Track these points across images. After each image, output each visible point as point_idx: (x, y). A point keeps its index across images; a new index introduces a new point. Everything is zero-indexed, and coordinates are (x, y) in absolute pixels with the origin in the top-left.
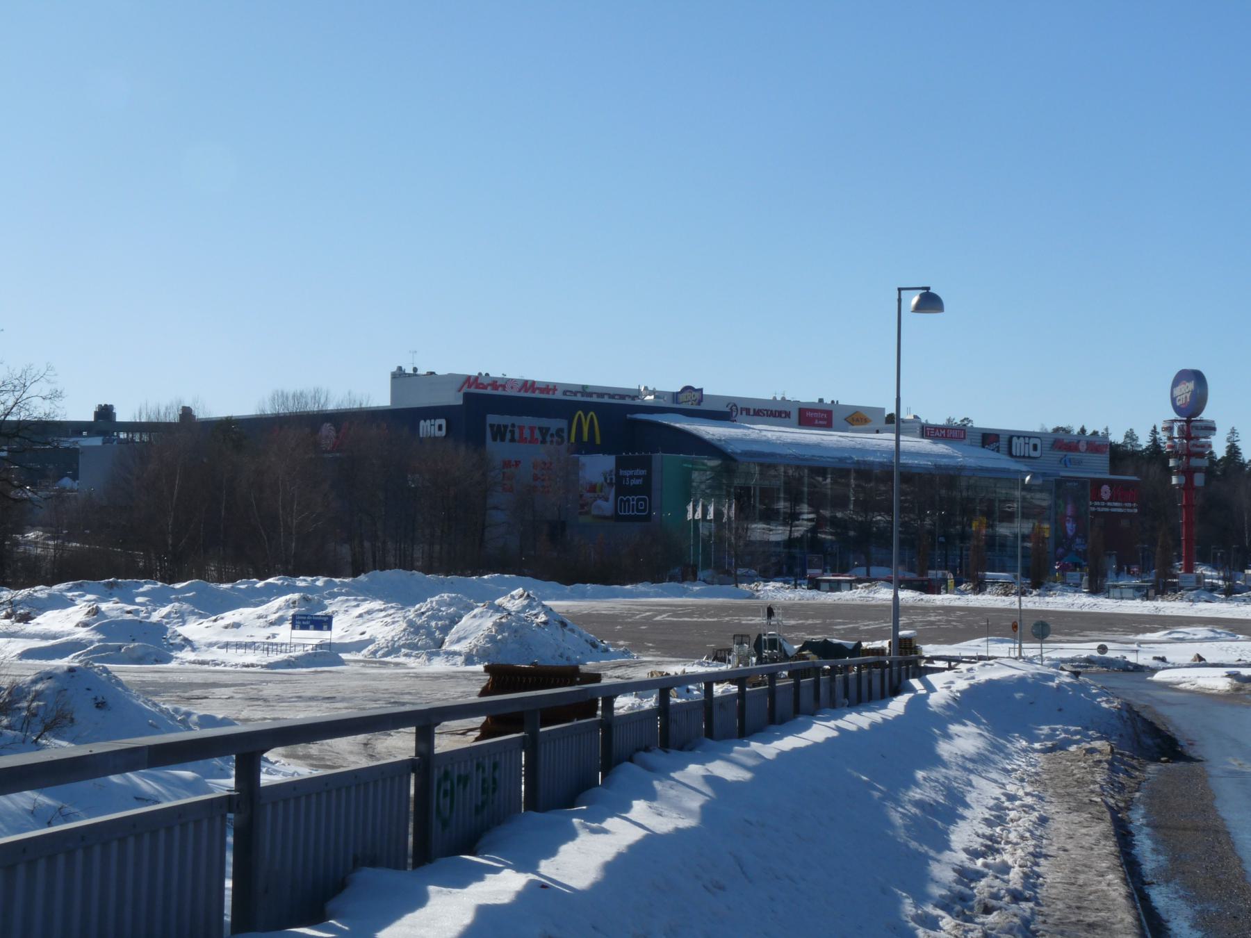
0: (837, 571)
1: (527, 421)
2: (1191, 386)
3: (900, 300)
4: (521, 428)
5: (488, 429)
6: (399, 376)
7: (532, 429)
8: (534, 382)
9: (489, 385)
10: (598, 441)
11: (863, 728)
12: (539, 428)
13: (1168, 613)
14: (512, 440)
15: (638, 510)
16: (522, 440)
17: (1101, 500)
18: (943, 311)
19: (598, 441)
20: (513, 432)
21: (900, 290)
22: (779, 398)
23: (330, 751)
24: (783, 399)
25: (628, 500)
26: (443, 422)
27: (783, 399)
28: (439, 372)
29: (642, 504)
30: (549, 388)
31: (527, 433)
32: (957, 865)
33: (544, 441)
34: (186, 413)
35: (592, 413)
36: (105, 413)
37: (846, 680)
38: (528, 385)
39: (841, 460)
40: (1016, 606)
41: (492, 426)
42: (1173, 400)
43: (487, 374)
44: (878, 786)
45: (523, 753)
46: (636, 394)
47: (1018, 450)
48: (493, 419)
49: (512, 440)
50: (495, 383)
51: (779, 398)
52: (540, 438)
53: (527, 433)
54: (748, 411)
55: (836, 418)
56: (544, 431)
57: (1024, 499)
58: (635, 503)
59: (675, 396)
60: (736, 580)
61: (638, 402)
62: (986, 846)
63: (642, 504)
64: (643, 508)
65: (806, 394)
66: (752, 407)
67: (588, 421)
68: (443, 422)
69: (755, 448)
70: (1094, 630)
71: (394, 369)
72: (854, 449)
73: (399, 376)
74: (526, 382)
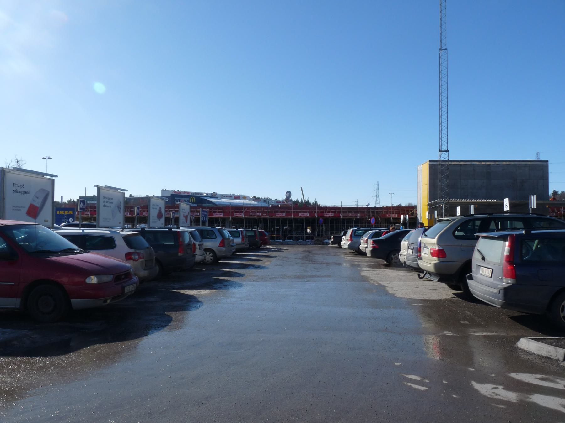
0: (408, 228)
1: (182, 199)
2: (289, 194)
5: (175, 201)
6: (163, 190)
10: (195, 202)
18: (80, 197)
19: (195, 202)
20: (179, 201)
30: (189, 193)
32: (317, 254)
34: (154, 195)
35: (194, 197)
36: (154, 195)
37: (271, 232)
38: (185, 192)
39: (237, 205)
40: (61, 211)
42: (286, 196)
46: (202, 194)
47: (532, 198)
48: (176, 198)
54: (225, 196)
61: (203, 195)
62: (305, 251)
65: (236, 193)
67: (193, 199)
69: (221, 203)
71: (162, 189)
72: (239, 203)
73: (163, 190)
74: (185, 192)
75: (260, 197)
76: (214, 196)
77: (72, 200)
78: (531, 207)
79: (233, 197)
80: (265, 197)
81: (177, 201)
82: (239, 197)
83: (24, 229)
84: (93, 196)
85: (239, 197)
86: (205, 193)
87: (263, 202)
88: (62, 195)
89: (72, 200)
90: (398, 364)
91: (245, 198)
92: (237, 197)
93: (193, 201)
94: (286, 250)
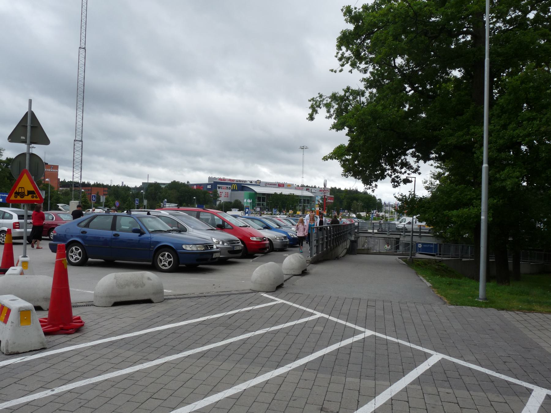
1: (224, 186)
5: (217, 187)
7: (225, 187)
10: (237, 189)
13: (394, 339)
14: (222, 189)
16: (223, 189)
19: (237, 189)
23: (340, 242)
26: (210, 186)
31: (224, 188)
33: (227, 189)
41: (218, 187)
44: (55, 328)
45: (473, 259)
46: (245, 181)
48: (218, 185)
49: (222, 189)
53: (224, 188)
56: (227, 187)
57: (304, 205)
60: (373, 228)
66: (270, 183)
68: (210, 186)
70: (468, 306)
75: (396, 188)
76: (258, 183)
77: (126, 186)
78: (204, 250)
79: (277, 185)
80: (312, 186)
81: (219, 188)
82: (284, 185)
83: (466, 210)
84: (154, 182)
85: (284, 185)
86: (248, 181)
87: (306, 190)
88: (123, 181)
89: (126, 186)
90: (472, 140)
91: (289, 186)
92: (281, 185)
93: (234, 189)
94: (464, 409)
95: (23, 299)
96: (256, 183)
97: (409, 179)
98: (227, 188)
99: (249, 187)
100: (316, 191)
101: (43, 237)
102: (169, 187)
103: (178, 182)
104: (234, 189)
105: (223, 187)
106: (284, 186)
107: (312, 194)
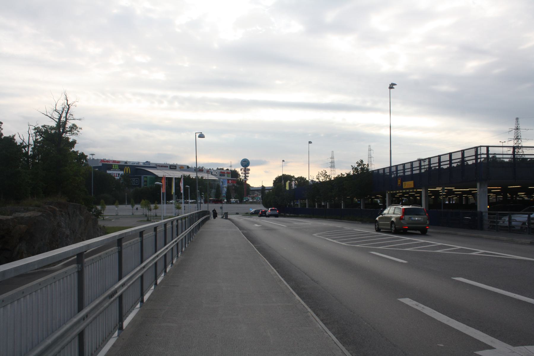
3: (196, 135)
4: (114, 174)
7: (116, 174)
8: (115, 161)
9: (106, 161)
11: (84, 154)
12: (118, 174)
15: (136, 183)
17: (229, 183)
21: (196, 133)
22: (165, 163)
24: (166, 163)
25: (132, 179)
27: (166, 163)
28: (95, 159)
29: (137, 181)
43: (105, 159)
50: (107, 161)
51: (165, 163)
52: (118, 176)
55: (177, 168)
58: (134, 181)
59: (144, 163)
63: (137, 181)
64: (137, 182)
74: (114, 161)
85: (176, 166)
93: (127, 172)
95: (500, 294)
96: (144, 164)
97: (504, 160)
98: (119, 175)
99: (146, 169)
100: (217, 173)
101: (76, 257)
102: (491, 156)
103: (276, 178)
104: (127, 172)
105: (114, 174)
106: (176, 169)
107: (215, 177)
